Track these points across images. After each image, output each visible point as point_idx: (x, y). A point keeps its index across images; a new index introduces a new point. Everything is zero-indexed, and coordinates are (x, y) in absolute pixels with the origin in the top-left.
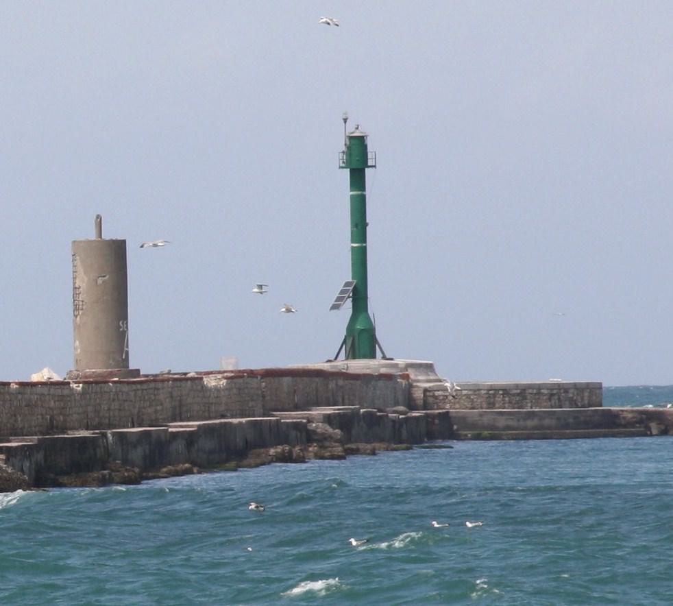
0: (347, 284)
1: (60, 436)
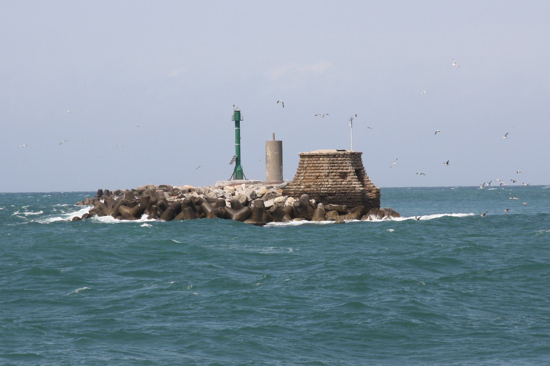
0: (234, 156)
1: (454, 215)
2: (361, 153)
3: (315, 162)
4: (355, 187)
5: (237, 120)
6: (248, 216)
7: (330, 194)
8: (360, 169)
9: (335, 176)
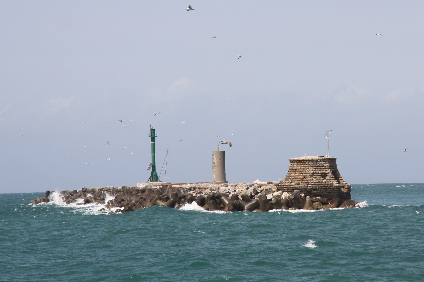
2: (336, 159)
3: (302, 165)
4: (333, 184)
5: (153, 136)
6: (256, 206)
7: (315, 190)
8: (335, 171)
9: (318, 176)
